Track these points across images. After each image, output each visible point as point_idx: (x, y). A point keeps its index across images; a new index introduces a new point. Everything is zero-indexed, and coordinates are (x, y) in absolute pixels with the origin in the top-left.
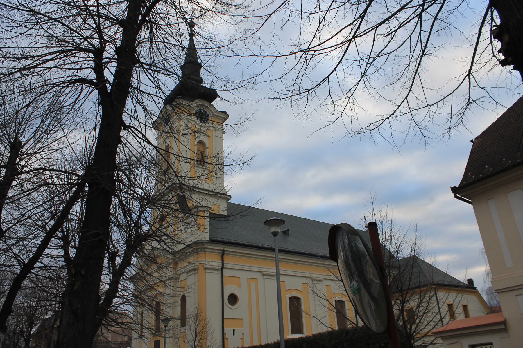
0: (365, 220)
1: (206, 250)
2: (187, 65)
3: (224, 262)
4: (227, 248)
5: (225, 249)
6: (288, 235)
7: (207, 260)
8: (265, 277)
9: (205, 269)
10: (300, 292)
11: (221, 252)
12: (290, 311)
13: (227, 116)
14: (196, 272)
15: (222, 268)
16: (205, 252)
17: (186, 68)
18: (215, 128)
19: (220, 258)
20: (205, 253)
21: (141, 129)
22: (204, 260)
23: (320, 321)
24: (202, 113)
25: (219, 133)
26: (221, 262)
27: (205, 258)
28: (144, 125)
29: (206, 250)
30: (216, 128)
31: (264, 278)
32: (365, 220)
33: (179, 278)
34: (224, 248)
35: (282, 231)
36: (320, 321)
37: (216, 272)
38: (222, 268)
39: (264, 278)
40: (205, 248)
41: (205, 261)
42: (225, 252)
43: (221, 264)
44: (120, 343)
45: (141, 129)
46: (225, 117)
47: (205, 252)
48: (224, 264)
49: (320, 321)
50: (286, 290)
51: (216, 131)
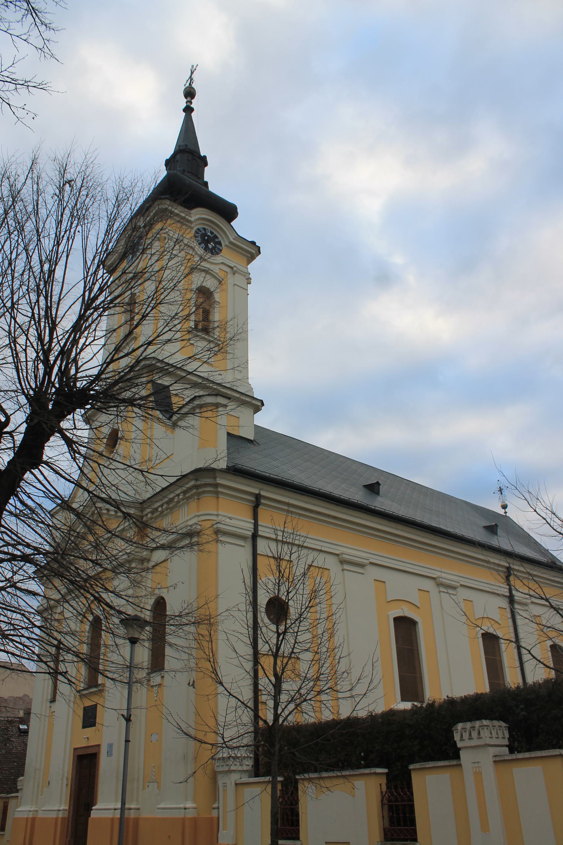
0: (501, 493)
1: (220, 489)
2: (178, 157)
3: (259, 523)
4: (268, 492)
5: (263, 493)
6: (378, 493)
7: (220, 513)
8: (346, 567)
9: (218, 532)
10: (415, 608)
11: (252, 498)
12: (397, 647)
13: (257, 249)
14: (195, 539)
15: (255, 536)
16: (217, 493)
17: (177, 161)
18: (232, 268)
19: (250, 513)
20: (218, 498)
21: (80, 298)
22: (215, 513)
23: (530, 653)
24: (208, 236)
25: (239, 279)
26: (253, 521)
27: (218, 510)
28: (71, 664)
29: (220, 489)
30: (235, 269)
31: (343, 570)
32: (501, 493)
33: (149, 560)
34: (261, 489)
35: (364, 486)
36: (530, 653)
37: (241, 543)
38: (255, 536)
39: (343, 570)
40: (216, 485)
41: (217, 515)
42: (262, 501)
43: (252, 526)
44: (7, 721)
45: (80, 298)
46: (254, 252)
47: (217, 493)
48: (260, 528)
49: (529, 651)
50: (389, 600)
51: (234, 274)
